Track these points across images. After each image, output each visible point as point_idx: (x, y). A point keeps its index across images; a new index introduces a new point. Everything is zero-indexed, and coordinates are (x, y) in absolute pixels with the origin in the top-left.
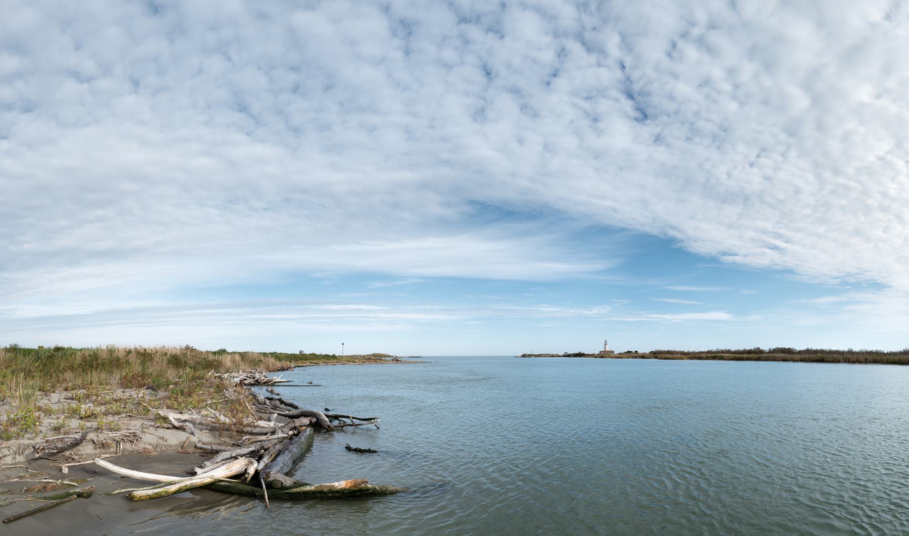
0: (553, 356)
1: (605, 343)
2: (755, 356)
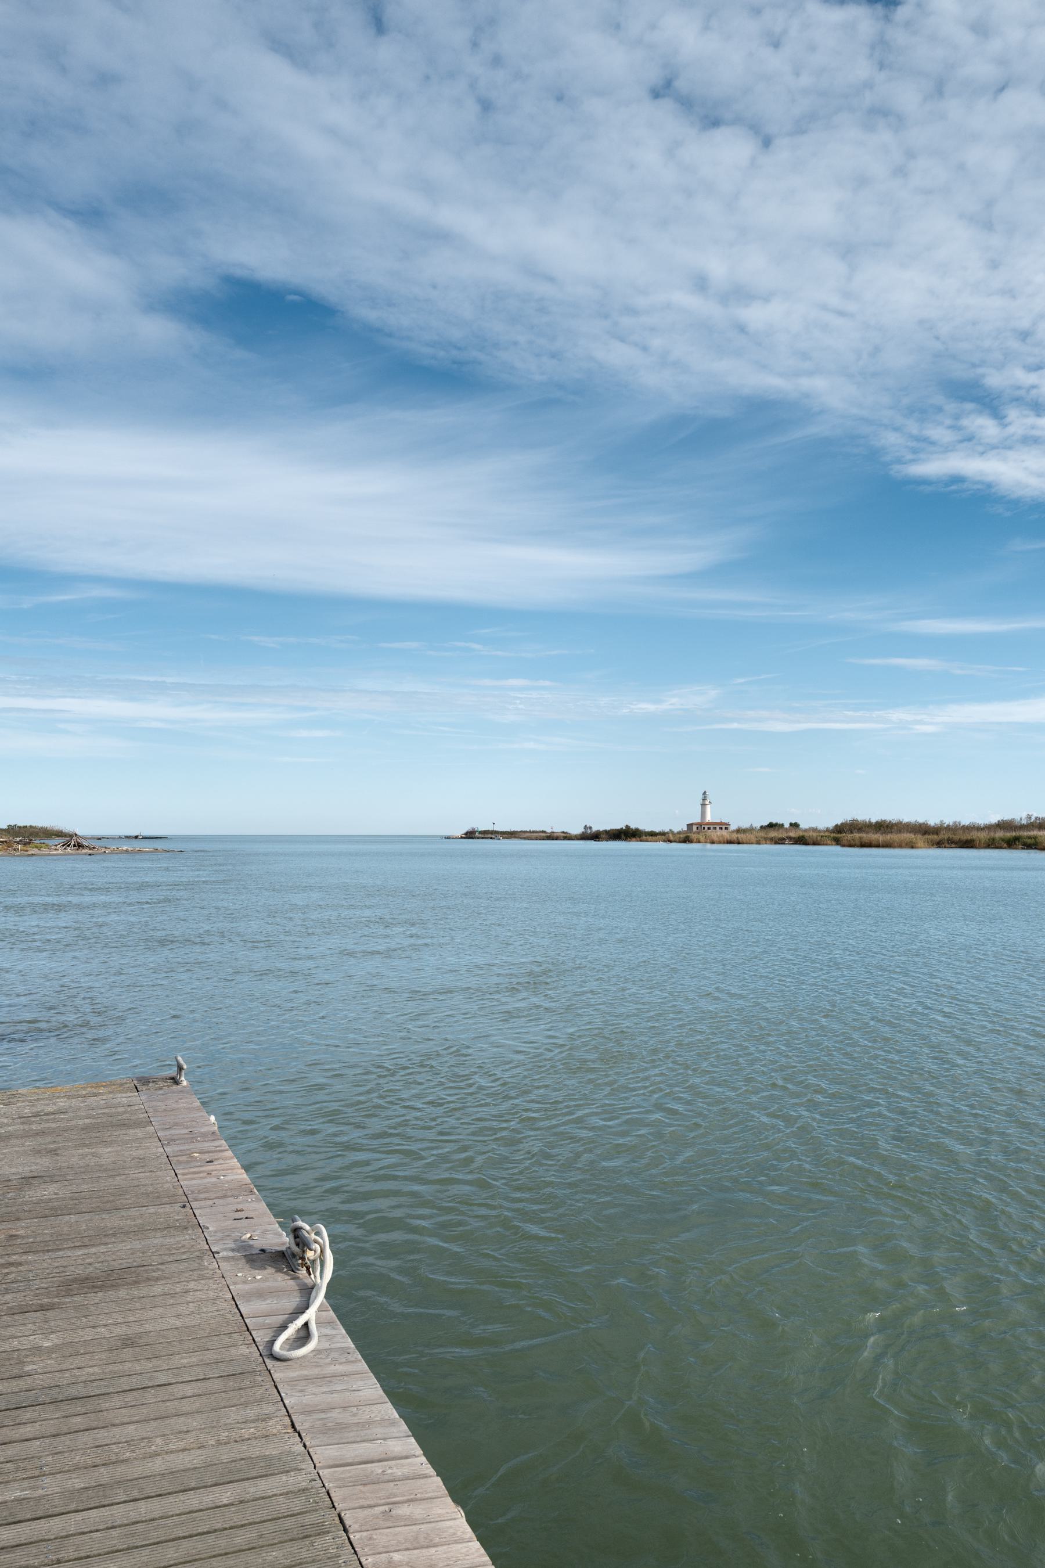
0: (551, 837)
1: (704, 800)
2: (894, 837)
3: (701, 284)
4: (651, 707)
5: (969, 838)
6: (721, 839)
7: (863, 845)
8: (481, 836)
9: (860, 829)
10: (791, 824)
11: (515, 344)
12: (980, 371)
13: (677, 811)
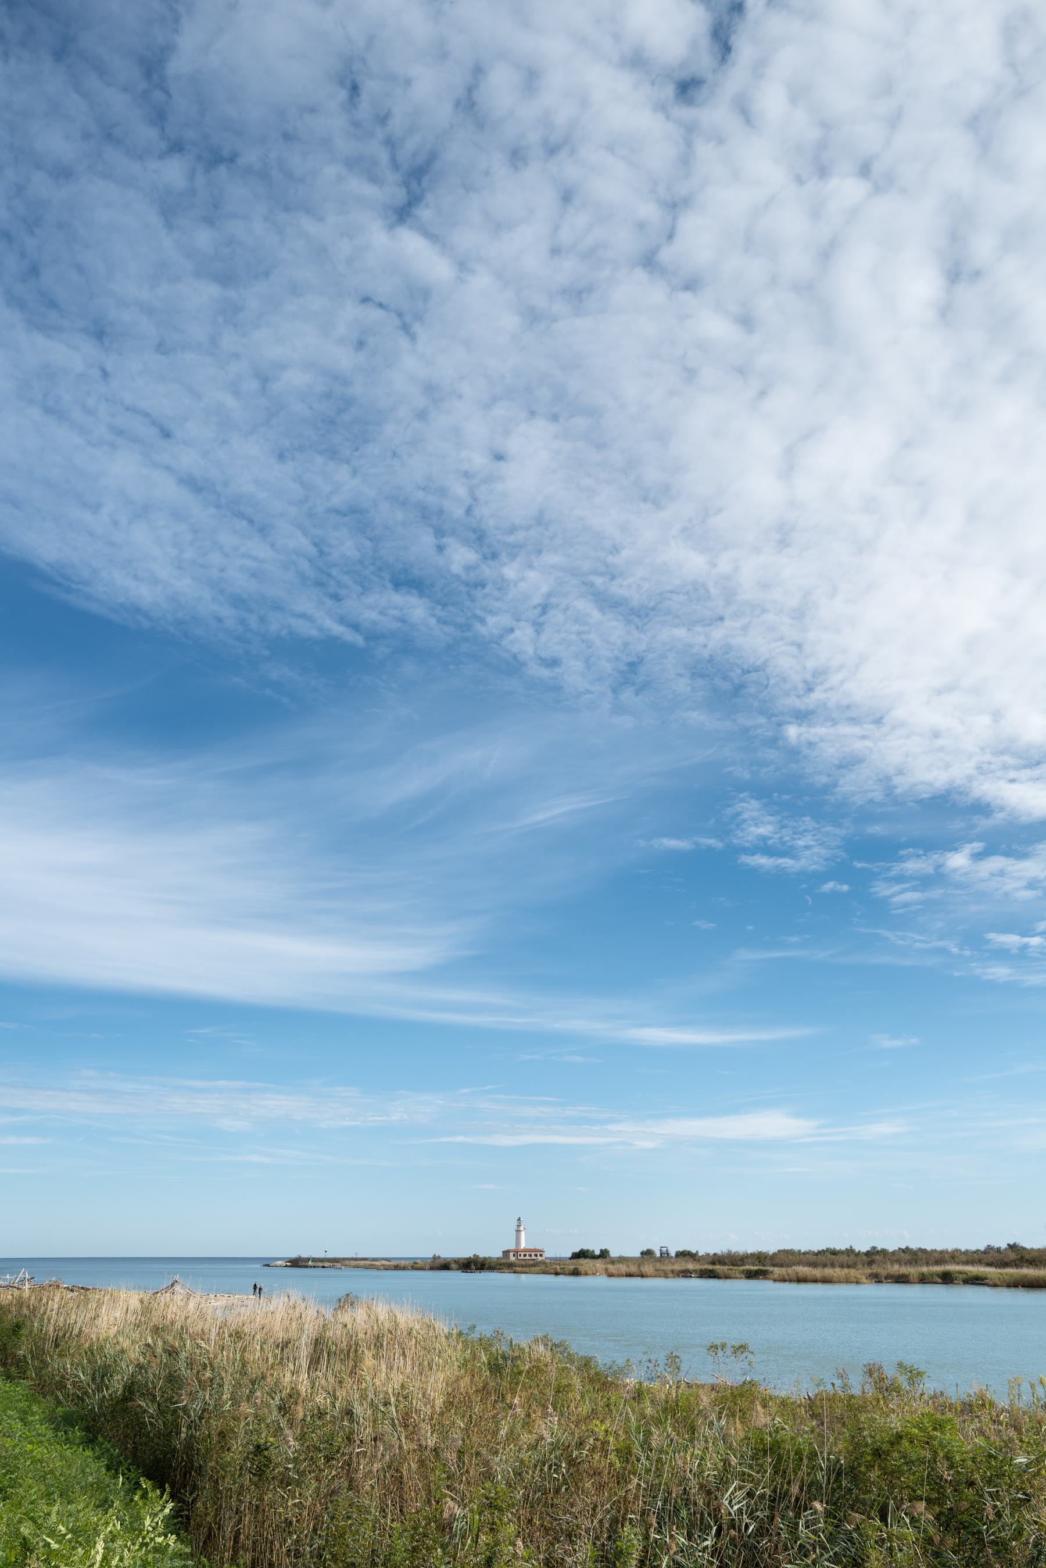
1: (519, 1226)
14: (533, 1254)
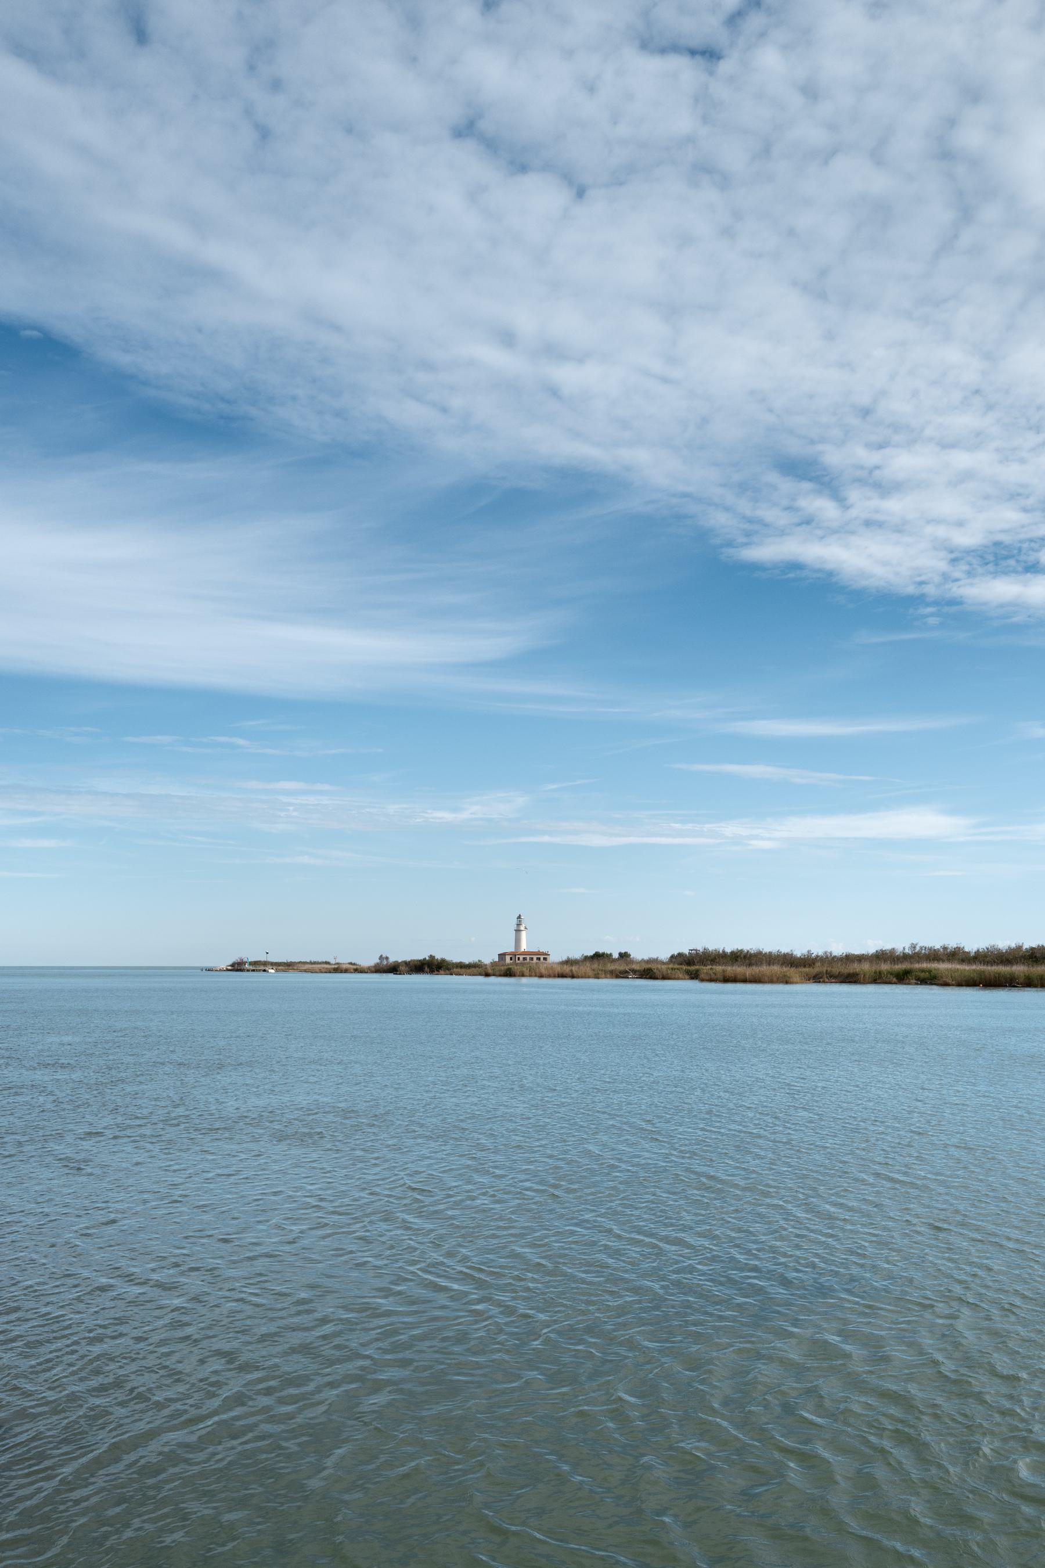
0: (338, 970)
1: (519, 925)
3: (507, 338)
4: (447, 816)
5: (852, 971)
6: (551, 972)
7: (726, 980)
8: (251, 968)
9: (712, 960)
10: (620, 954)
11: (294, 398)
12: (819, 447)
13: (473, 939)
14: (535, 957)
